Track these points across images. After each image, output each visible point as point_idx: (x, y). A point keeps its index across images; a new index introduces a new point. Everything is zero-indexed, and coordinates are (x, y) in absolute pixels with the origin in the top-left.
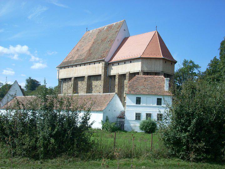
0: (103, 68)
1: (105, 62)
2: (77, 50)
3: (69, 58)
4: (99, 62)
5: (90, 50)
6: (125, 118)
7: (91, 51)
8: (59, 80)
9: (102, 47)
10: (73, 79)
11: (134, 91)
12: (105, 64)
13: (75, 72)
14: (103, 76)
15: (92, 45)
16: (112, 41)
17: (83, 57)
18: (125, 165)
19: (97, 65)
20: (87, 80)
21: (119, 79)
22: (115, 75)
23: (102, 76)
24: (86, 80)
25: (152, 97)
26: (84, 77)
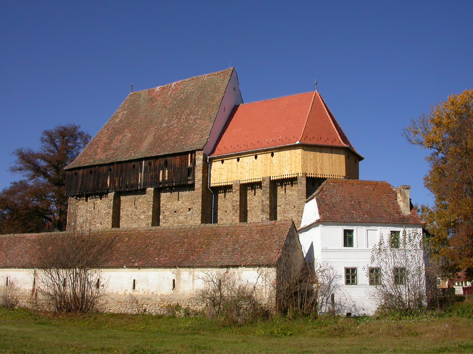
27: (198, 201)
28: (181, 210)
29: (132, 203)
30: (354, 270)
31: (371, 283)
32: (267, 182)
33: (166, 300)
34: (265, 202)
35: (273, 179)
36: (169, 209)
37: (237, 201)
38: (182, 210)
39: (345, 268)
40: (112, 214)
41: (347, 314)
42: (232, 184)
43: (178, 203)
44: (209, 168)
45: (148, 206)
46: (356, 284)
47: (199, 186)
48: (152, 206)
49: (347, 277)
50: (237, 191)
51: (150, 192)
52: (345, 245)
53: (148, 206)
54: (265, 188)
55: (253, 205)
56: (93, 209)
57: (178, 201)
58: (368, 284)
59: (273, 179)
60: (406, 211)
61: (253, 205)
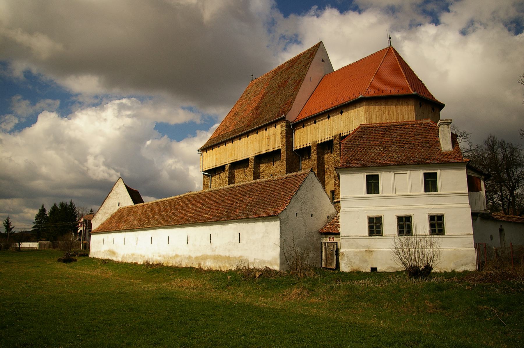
0: (284, 134)
1: (287, 122)
2: (235, 114)
3: (220, 131)
4: (274, 123)
5: (257, 108)
6: (339, 233)
7: (260, 109)
8: (204, 174)
9: (280, 97)
10: (227, 168)
11: (359, 160)
12: (288, 126)
13: (231, 154)
14: (283, 151)
15: (262, 98)
16: (299, 82)
17: (246, 122)
18: (469, 27)
19: (271, 130)
20: (254, 165)
21: (318, 153)
22: (310, 147)
23: (282, 152)
24: (251, 165)
25: (408, 172)
26: (248, 159)
27: (283, 163)
28: (275, 174)
29: (243, 171)
30: (440, 218)
31: (401, 233)
32: (337, 139)
33: (111, 264)
34: (336, 159)
35: (343, 136)
36: (267, 173)
37: (315, 161)
38: (276, 173)
39: (368, 217)
40: (228, 182)
41: (371, 268)
42: (311, 145)
43: (273, 167)
44: (293, 133)
45: (250, 172)
46: (382, 235)
47: (283, 150)
48: (253, 172)
49: (432, 226)
50: (315, 151)
51: (252, 161)
52: (369, 192)
53: (250, 172)
54: (336, 145)
55: (331, 163)
56: (219, 179)
57: (274, 165)
58: (397, 234)
59: (343, 136)
60: (446, 146)
61: (331, 163)
